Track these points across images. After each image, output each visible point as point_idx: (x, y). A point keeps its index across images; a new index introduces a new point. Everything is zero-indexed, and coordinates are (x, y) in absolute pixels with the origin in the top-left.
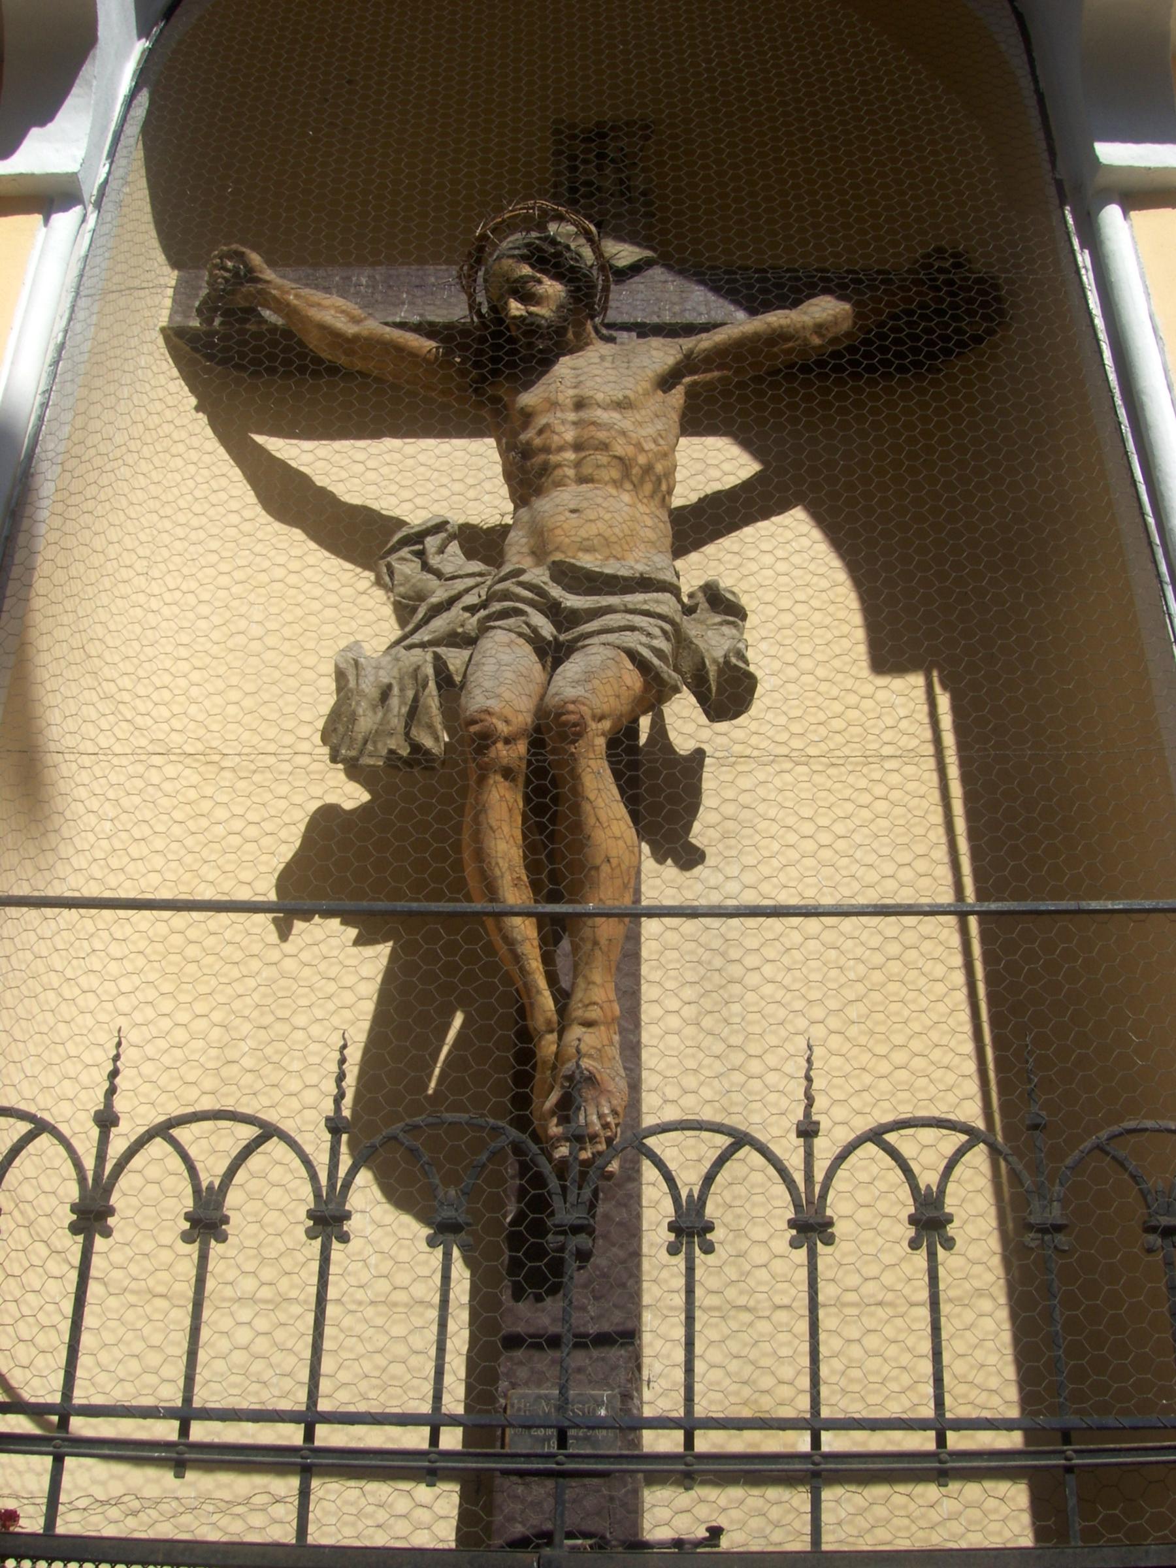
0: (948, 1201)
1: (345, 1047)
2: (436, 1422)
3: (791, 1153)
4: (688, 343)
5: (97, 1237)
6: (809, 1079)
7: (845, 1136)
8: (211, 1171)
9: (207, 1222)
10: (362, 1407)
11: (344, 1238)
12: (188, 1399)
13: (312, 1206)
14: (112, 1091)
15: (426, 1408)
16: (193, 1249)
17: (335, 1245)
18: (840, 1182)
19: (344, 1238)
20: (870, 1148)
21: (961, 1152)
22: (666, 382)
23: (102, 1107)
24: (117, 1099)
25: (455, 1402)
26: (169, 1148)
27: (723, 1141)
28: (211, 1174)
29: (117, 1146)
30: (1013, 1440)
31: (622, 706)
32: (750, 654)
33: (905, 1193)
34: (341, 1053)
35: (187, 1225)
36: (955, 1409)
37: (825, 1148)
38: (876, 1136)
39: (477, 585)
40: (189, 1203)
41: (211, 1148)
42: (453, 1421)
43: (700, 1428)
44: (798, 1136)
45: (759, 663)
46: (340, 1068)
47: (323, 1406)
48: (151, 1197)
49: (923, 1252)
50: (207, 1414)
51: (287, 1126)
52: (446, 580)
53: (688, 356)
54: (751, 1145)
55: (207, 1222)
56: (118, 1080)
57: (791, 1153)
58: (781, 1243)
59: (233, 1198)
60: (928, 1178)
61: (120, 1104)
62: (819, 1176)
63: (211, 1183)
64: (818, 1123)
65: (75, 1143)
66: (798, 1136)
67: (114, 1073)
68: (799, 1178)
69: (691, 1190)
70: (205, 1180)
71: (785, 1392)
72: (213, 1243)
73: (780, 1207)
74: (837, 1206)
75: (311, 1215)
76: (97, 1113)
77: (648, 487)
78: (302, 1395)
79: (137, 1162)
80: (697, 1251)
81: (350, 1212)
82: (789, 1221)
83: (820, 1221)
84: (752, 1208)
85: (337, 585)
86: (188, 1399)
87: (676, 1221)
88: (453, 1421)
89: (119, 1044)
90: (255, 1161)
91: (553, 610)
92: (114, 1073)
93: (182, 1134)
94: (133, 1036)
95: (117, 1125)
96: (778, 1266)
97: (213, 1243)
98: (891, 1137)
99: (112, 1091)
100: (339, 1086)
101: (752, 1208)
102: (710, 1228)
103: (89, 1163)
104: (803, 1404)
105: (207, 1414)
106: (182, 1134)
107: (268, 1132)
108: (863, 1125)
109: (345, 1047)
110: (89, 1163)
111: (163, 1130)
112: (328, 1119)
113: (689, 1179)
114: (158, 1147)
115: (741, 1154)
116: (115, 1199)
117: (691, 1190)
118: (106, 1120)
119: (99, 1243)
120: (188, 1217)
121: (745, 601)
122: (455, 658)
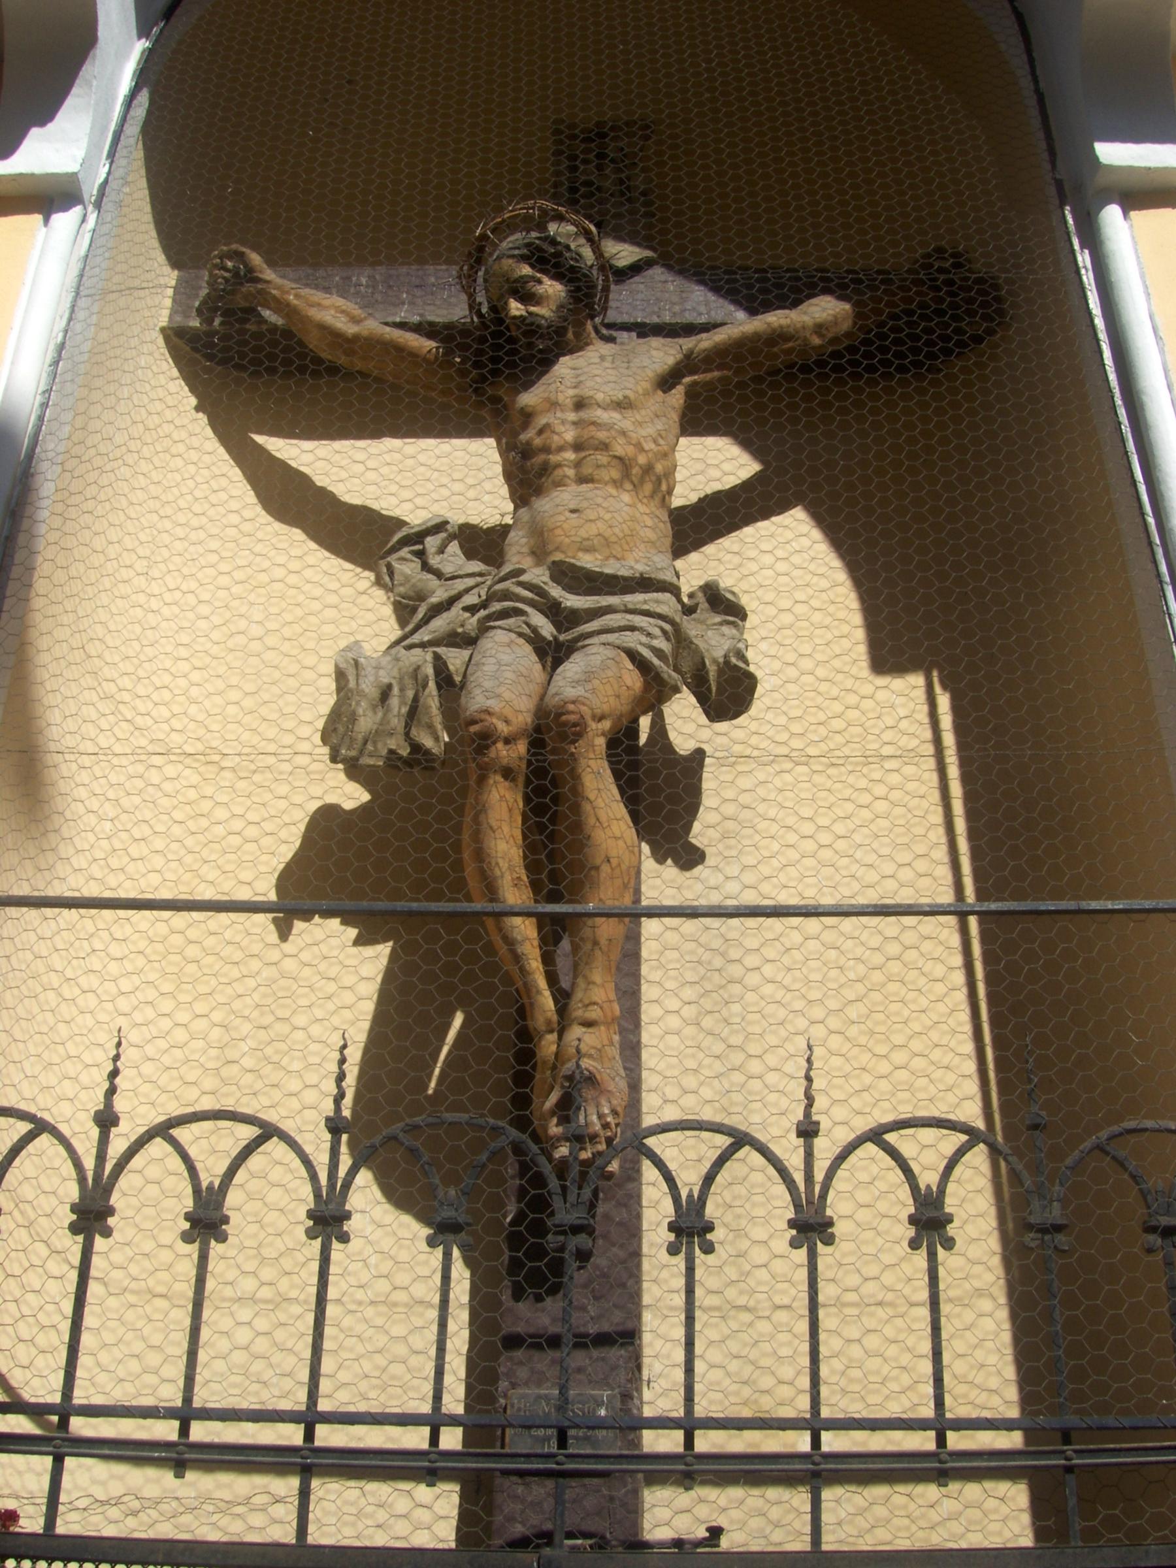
0: (948, 1201)
1: (345, 1047)
2: (436, 1422)
3: (791, 1153)
4: (688, 343)
5: (97, 1237)
6: (809, 1079)
7: (845, 1136)
8: (211, 1171)
9: (207, 1222)
10: (362, 1407)
11: (344, 1238)
12: (188, 1399)
13: (312, 1206)
14: (112, 1091)
15: (426, 1408)
16: (193, 1249)
17: (335, 1245)
18: (840, 1182)
19: (344, 1238)
20: (870, 1148)
21: (961, 1152)
22: (666, 382)
23: (102, 1107)
24: (117, 1099)
25: (455, 1402)
26: (169, 1148)
27: (723, 1141)
28: (211, 1174)
29: (117, 1146)
30: (1013, 1440)
31: (622, 706)
32: (750, 654)
33: (905, 1193)
34: (341, 1053)
35: (187, 1225)
36: (955, 1409)
37: (825, 1148)
38: (876, 1136)
39: (477, 585)
40: (189, 1203)
41: (211, 1148)
42: (453, 1421)
43: (700, 1428)
44: (798, 1136)
45: (759, 663)
46: (340, 1068)
47: (323, 1406)
48: (151, 1197)
49: (923, 1252)
50: (207, 1414)
51: (287, 1126)
52: (446, 580)
53: (688, 356)
54: (751, 1145)
55: (207, 1222)
56: (118, 1080)
57: (791, 1153)
58: (781, 1243)
59: (233, 1198)
60: (928, 1178)
61: (120, 1104)
62: (819, 1176)
63: (211, 1183)
64: (818, 1123)
65: (75, 1143)
66: (798, 1136)
67: (114, 1073)
68: (799, 1178)
69: (691, 1190)
70: (205, 1180)
71: (785, 1392)
72: (213, 1243)
73: (780, 1207)
74: (837, 1206)
75: (311, 1215)
76: (97, 1113)
77: (648, 487)
78: (302, 1395)
79: (137, 1162)
80: (697, 1251)
81: (350, 1212)
82: (789, 1221)
83: (820, 1221)
84: (752, 1208)
85: (337, 585)
86: (188, 1399)
87: (676, 1221)
88: (453, 1421)
89: (119, 1044)
90: (255, 1161)
91: (553, 610)
92: (114, 1073)
93: (182, 1134)
94: (133, 1036)
95: (117, 1125)
96: (778, 1266)
97: (213, 1243)
98: (891, 1137)
99: (112, 1091)
100: (339, 1086)
101: (752, 1208)
102: (710, 1228)
103: (89, 1163)
104: (803, 1404)
105: (207, 1414)
106: (182, 1134)
107: (268, 1132)
108: (863, 1125)
109: (345, 1047)
110: (89, 1163)
111: (163, 1130)
112: (328, 1119)
113: (689, 1179)
114: (158, 1147)
115: (741, 1154)
116: (115, 1199)
117: (691, 1190)
118: (106, 1120)
119: (99, 1243)
120: (188, 1217)
121: (745, 601)
122: (455, 658)
